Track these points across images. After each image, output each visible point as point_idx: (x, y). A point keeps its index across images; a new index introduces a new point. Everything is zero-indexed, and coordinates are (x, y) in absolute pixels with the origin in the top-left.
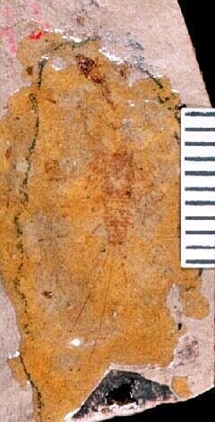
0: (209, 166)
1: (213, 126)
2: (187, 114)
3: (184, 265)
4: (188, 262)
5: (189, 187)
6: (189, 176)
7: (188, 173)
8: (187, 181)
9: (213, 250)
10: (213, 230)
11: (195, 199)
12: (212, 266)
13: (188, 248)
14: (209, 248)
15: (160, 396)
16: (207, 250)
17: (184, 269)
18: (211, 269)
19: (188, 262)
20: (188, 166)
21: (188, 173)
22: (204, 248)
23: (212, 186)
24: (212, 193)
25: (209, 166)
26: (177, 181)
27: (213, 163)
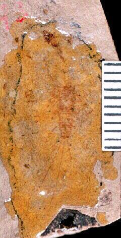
0: (118, 94)
1: (120, 71)
2: (105, 64)
3: (103, 149)
4: (106, 148)
5: (106, 105)
6: (106, 99)
7: (106, 98)
8: (105, 102)
9: (120, 141)
10: (120, 130)
11: (110, 112)
12: (119, 150)
13: (106, 140)
14: (117, 140)
15: (90, 223)
16: (116, 141)
17: (104, 152)
18: (119, 152)
19: (106, 148)
20: (106, 94)
21: (106, 98)
22: (115, 140)
23: (119, 105)
24: (120, 109)
25: (118, 94)
26: (100, 102)
27: (120, 92)
